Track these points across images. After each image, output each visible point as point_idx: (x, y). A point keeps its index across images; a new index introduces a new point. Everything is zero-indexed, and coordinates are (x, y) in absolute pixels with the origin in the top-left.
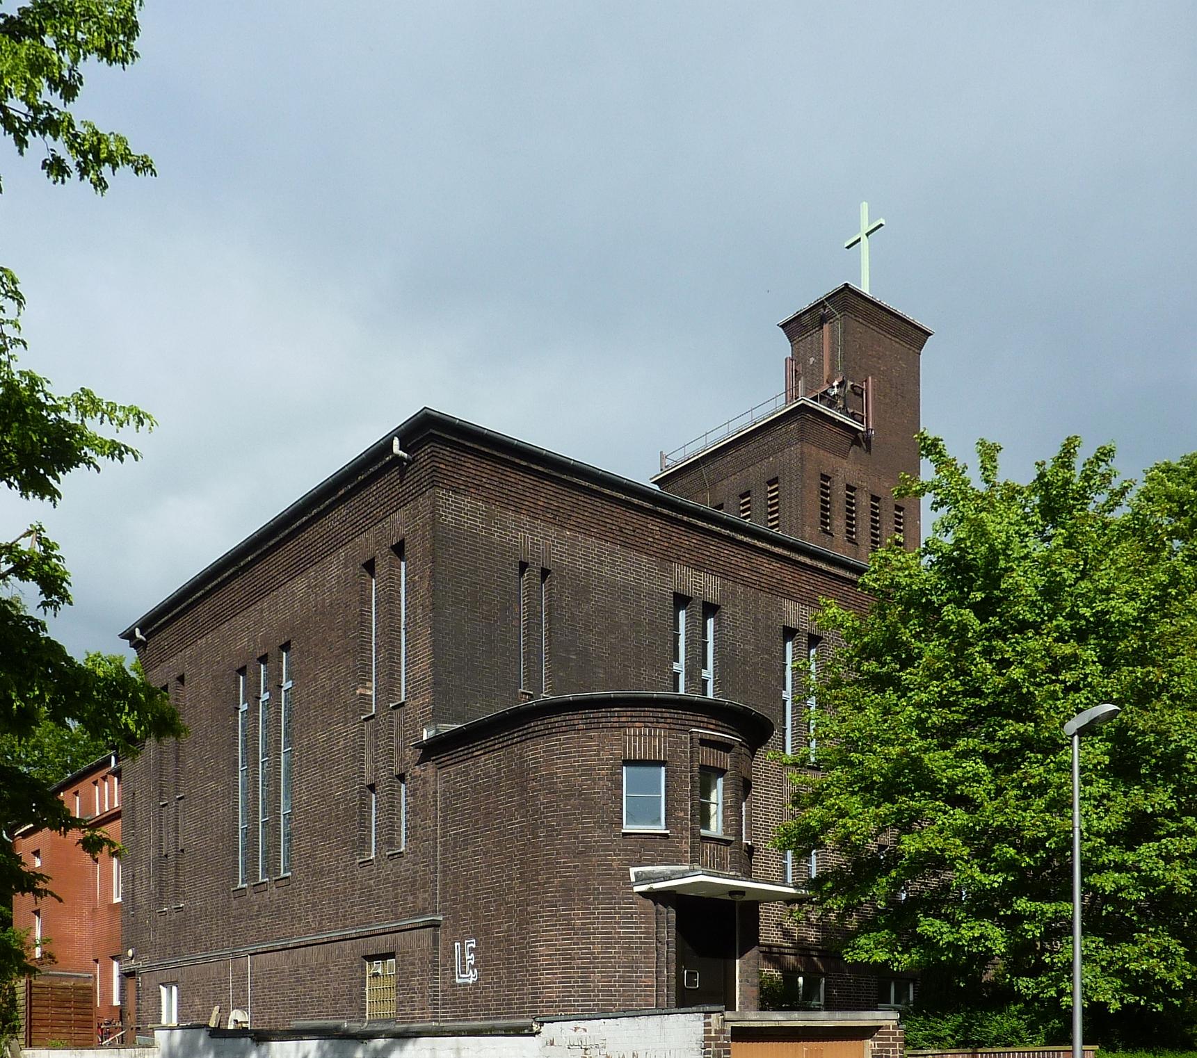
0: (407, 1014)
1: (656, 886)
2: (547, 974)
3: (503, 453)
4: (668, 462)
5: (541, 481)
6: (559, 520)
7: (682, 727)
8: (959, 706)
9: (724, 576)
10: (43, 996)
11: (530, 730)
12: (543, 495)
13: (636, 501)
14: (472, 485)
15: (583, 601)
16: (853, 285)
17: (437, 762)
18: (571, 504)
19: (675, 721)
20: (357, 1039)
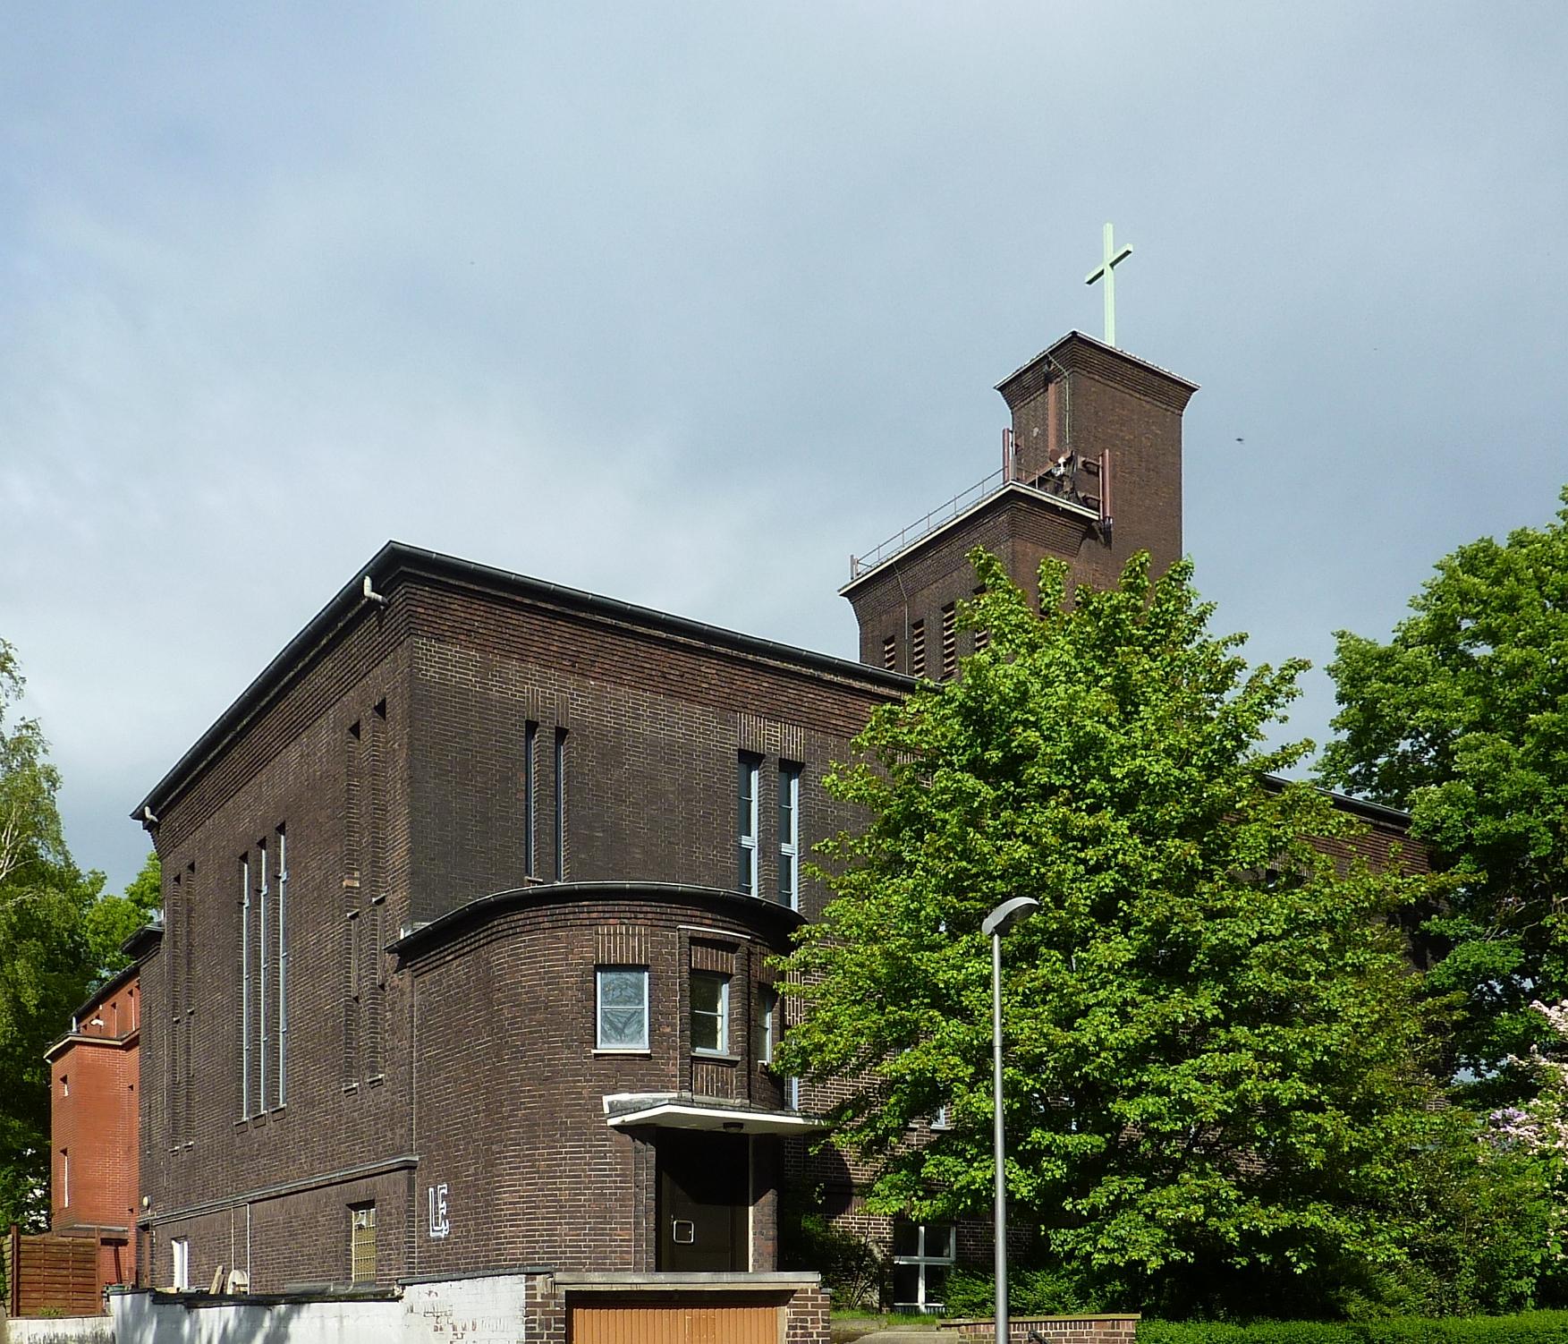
0: (384, 1275)
1: (629, 1118)
2: (511, 1226)
3: (500, 591)
4: (860, 568)
5: (553, 621)
6: (578, 667)
7: (668, 924)
8: (976, 892)
9: (810, 726)
10: (33, 1255)
11: (494, 930)
12: (556, 638)
13: (681, 639)
14: (461, 631)
15: (612, 766)
16: (1084, 333)
17: (413, 968)
18: (596, 648)
19: (658, 916)
20: (262, 1305)
